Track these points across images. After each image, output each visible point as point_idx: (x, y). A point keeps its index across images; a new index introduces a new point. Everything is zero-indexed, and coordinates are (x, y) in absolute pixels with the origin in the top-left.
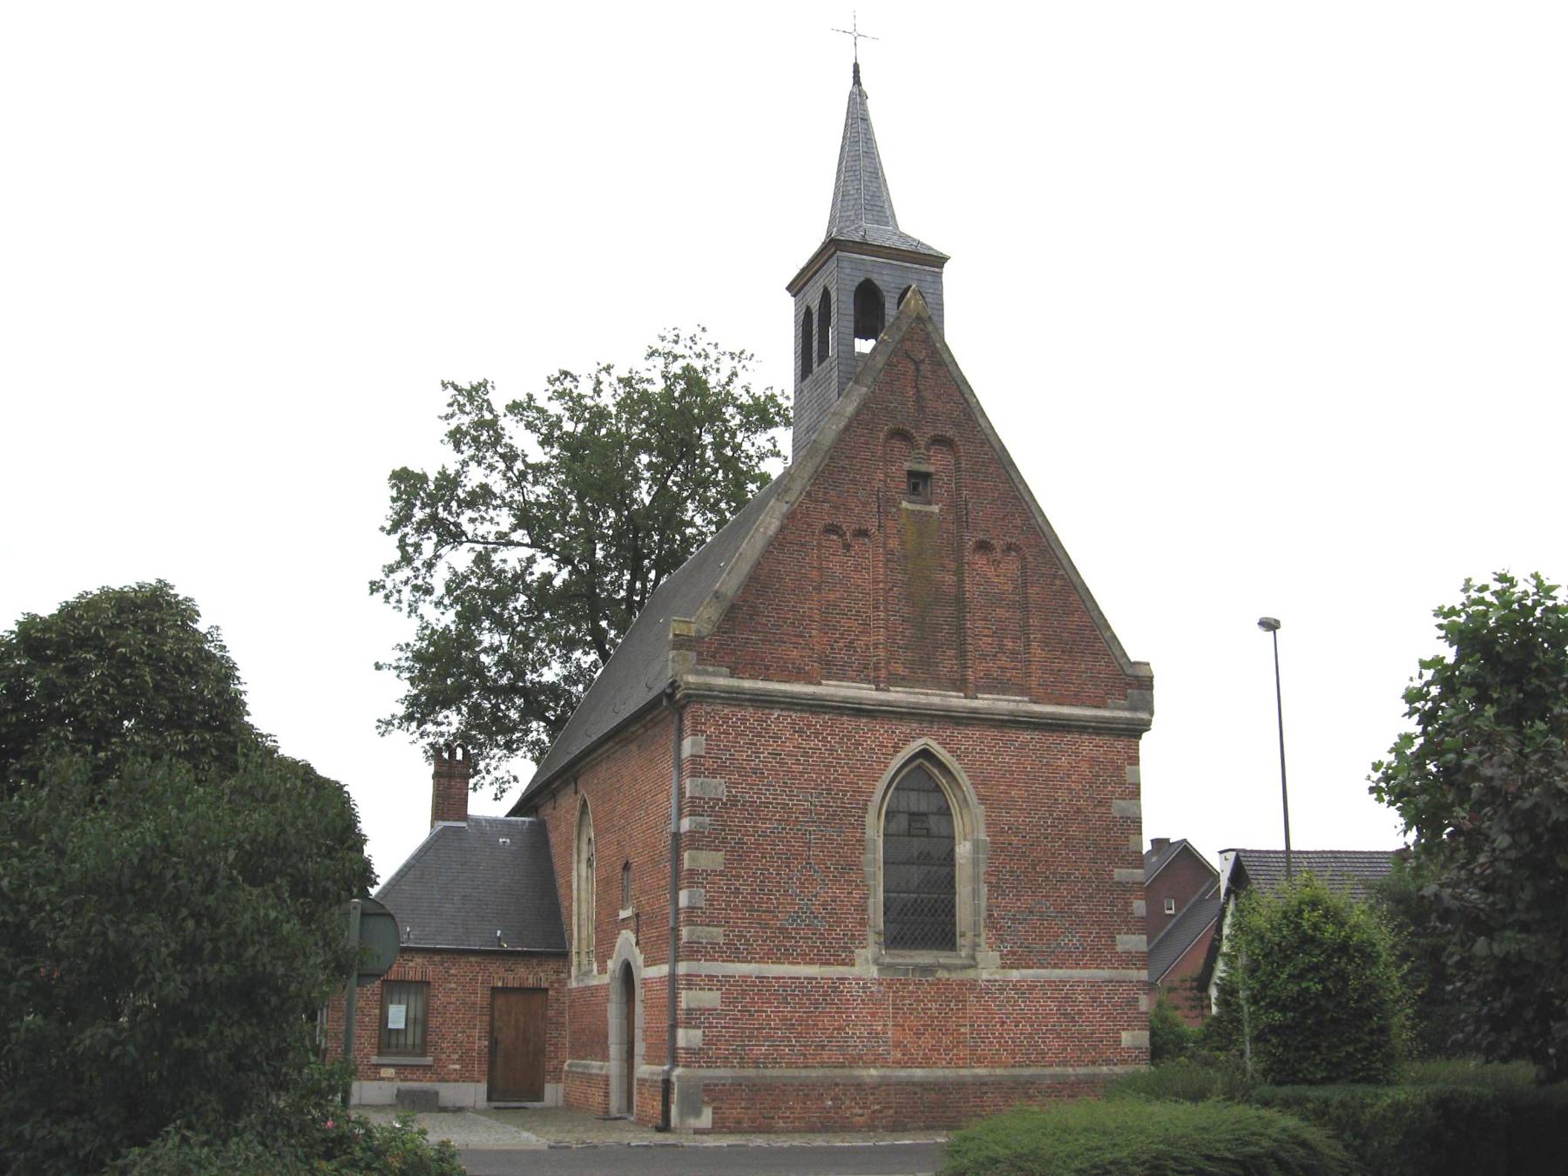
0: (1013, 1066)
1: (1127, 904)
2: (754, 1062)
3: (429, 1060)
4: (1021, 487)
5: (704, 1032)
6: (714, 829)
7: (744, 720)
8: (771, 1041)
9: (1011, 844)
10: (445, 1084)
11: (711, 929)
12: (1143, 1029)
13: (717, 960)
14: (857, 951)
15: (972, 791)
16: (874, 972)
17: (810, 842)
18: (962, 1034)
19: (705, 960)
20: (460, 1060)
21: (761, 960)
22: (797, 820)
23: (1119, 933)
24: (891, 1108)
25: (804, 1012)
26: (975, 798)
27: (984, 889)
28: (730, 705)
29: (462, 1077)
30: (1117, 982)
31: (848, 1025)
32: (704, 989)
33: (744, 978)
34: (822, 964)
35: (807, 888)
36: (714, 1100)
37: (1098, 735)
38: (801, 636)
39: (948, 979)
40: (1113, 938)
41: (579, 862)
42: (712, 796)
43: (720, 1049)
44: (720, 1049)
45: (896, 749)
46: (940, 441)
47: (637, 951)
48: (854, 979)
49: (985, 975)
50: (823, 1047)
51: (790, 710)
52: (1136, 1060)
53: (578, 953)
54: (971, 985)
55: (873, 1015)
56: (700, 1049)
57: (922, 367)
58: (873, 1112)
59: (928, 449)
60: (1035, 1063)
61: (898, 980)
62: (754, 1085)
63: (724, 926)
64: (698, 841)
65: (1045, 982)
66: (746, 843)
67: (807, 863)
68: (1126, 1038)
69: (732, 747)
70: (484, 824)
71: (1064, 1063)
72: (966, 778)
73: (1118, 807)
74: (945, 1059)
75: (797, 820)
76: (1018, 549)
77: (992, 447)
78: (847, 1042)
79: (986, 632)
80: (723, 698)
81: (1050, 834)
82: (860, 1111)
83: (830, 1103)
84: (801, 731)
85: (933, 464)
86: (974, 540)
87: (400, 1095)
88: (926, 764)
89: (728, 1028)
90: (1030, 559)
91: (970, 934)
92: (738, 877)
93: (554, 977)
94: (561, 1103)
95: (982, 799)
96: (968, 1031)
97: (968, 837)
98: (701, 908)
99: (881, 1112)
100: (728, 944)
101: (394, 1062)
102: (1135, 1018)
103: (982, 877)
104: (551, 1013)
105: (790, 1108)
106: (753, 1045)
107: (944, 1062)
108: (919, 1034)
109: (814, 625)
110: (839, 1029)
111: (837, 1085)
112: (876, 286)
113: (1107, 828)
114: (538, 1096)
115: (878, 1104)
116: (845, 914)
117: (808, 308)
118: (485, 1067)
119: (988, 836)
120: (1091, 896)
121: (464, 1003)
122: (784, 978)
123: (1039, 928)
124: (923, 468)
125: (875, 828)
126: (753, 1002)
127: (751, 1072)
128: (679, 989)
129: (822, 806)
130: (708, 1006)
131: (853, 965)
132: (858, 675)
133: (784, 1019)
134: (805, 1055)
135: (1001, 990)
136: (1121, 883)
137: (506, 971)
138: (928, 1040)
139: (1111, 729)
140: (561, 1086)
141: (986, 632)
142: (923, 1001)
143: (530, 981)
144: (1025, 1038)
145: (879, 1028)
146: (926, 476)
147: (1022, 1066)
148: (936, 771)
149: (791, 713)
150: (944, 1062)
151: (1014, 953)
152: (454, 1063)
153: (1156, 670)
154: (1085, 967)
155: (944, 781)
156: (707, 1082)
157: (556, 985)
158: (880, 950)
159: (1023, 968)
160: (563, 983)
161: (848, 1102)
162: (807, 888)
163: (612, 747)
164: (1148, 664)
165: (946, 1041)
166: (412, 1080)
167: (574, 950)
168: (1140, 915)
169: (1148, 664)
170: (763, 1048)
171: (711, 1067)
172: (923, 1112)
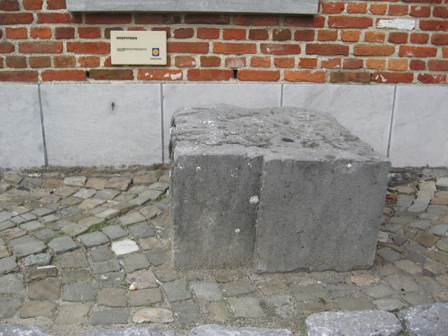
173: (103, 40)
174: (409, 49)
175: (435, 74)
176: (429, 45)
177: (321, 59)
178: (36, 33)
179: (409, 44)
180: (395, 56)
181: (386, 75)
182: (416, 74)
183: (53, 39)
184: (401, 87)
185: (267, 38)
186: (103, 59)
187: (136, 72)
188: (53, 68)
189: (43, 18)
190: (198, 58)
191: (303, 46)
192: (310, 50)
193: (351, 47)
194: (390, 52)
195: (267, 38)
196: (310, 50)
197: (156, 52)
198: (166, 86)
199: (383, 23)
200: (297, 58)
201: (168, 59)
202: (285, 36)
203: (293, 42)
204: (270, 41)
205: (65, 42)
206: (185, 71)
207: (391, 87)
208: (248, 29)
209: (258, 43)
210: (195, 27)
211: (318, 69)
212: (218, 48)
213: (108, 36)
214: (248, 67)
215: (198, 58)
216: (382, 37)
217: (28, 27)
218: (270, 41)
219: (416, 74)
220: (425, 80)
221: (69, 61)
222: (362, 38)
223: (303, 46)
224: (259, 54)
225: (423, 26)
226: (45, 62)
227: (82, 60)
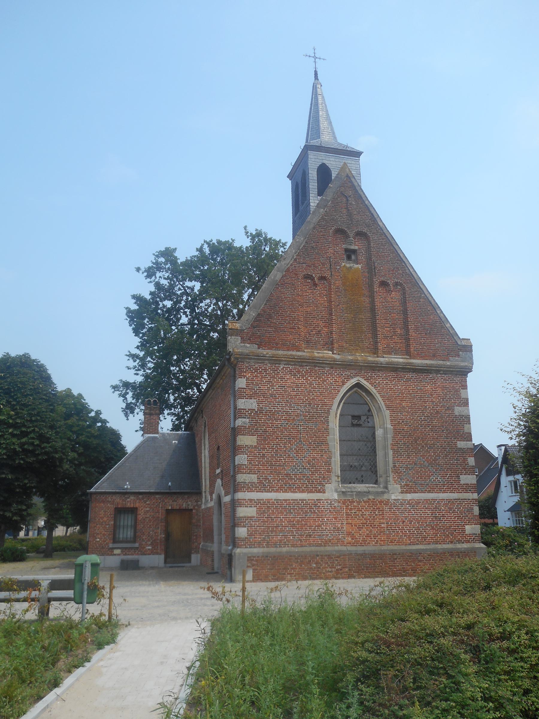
0: (410, 544)
1: (465, 460)
2: (274, 544)
3: (137, 545)
4: (401, 255)
5: (248, 529)
6: (251, 425)
7: (265, 370)
8: (283, 533)
9: (404, 430)
10: (144, 556)
11: (251, 475)
12: (476, 524)
13: (254, 491)
14: (326, 485)
15: (383, 403)
16: (336, 496)
17: (301, 431)
18: (382, 528)
19: (248, 492)
20: (152, 544)
21: (277, 491)
22: (294, 419)
23: (461, 474)
24: (346, 567)
25: (299, 518)
26: (384, 407)
27: (391, 453)
28: (258, 363)
29: (152, 552)
30: (461, 500)
31: (323, 524)
32: (247, 507)
33: (268, 500)
34: (308, 492)
35: (300, 453)
36: (253, 565)
37: (446, 374)
38: (294, 329)
39: (374, 499)
40: (458, 477)
41: (205, 449)
42: (250, 408)
43: (257, 538)
44: (257, 538)
45: (344, 383)
46: (360, 234)
47: (222, 489)
48: (325, 500)
49: (393, 497)
50: (310, 536)
51: (288, 364)
52: (474, 541)
53: (205, 492)
54: (386, 502)
55: (336, 518)
56: (246, 538)
57: (350, 199)
58: (337, 570)
59: (355, 238)
60: (421, 543)
61: (348, 500)
62: (275, 557)
63: (258, 474)
64: (243, 431)
65: (424, 500)
66: (268, 432)
67: (299, 441)
68: (469, 529)
69: (260, 383)
70: (166, 435)
71: (437, 543)
72: (379, 397)
73: (458, 410)
74: (374, 541)
75: (294, 419)
76: (401, 285)
77: (386, 236)
78: (322, 533)
79: (387, 325)
80: (254, 359)
81: (424, 424)
82: (330, 570)
83: (315, 565)
84: (295, 375)
85: (357, 245)
86: (379, 280)
87: (122, 562)
88: (359, 390)
89: (260, 526)
90: (407, 289)
91: (384, 476)
92: (264, 448)
93: (195, 504)
94: (199, 564)
95: (388, 407)
96: (385, 526)
97: (382, 427)
98: (246, 465)
99: (341, 570)
100: (260, 482)
101: (120, 546)
102: (472, 518)
103: (390, 447)
104: (194, 521)
105: (293, 569)
106: (274, 535)
107: (374, 543)
108: (360, 528)
109: (300, 323)
110: (319, 526)
111: (318, 556)
112: (328, 166)
113: (453, 421)
114: (190, 561)
115: (340, 565)
116: (320, 466)
117: (297, 183)
118: (163, 547)
119: (392, 426)
120: (446, 456)
121: (153, 517)
122: (289, 500)
123: (420, 472)
124: (353, 247)
125: (334, 423)
126: (273, 513)
127: (272, 550)
128: (235, 507)
129: (306, 412)
130: (250, 515)
131: (324, 493)
132: (323, 347)
133: (290, 521)
134: (301, 540)
135: (402, 504)
136: (461, 448)
137: (173, 501)
138: (365, 531)
139: (452, 371)
140: (199, 555)
141: (387, 325)
142: (361, 511)
143: (184, 506)
144: (415, 529)
145: (339, 525)
146: (354, 252)
147: (415, 545)
148: (364, 394)
149: (290, 366)
150: (374, 543)
151: (407, 485)
152: (149, 546)
153: (473, 342)
154: (444, 492)
155: (368, 399)
156: (249, 555)
157: (196, 507)
158: (339, 485)
159: (412, 493)
160: (200, 506)
161: (324, 565)
162: (300, 453)
163: (212, 392)
164: (469, 339)
165: (375, 531)
166: (129, 555)
167: (203, 490)
168: (472, 465)
169: (469, 339)
170: (279, 537)
171: (252, 547)
172: (363, 569)
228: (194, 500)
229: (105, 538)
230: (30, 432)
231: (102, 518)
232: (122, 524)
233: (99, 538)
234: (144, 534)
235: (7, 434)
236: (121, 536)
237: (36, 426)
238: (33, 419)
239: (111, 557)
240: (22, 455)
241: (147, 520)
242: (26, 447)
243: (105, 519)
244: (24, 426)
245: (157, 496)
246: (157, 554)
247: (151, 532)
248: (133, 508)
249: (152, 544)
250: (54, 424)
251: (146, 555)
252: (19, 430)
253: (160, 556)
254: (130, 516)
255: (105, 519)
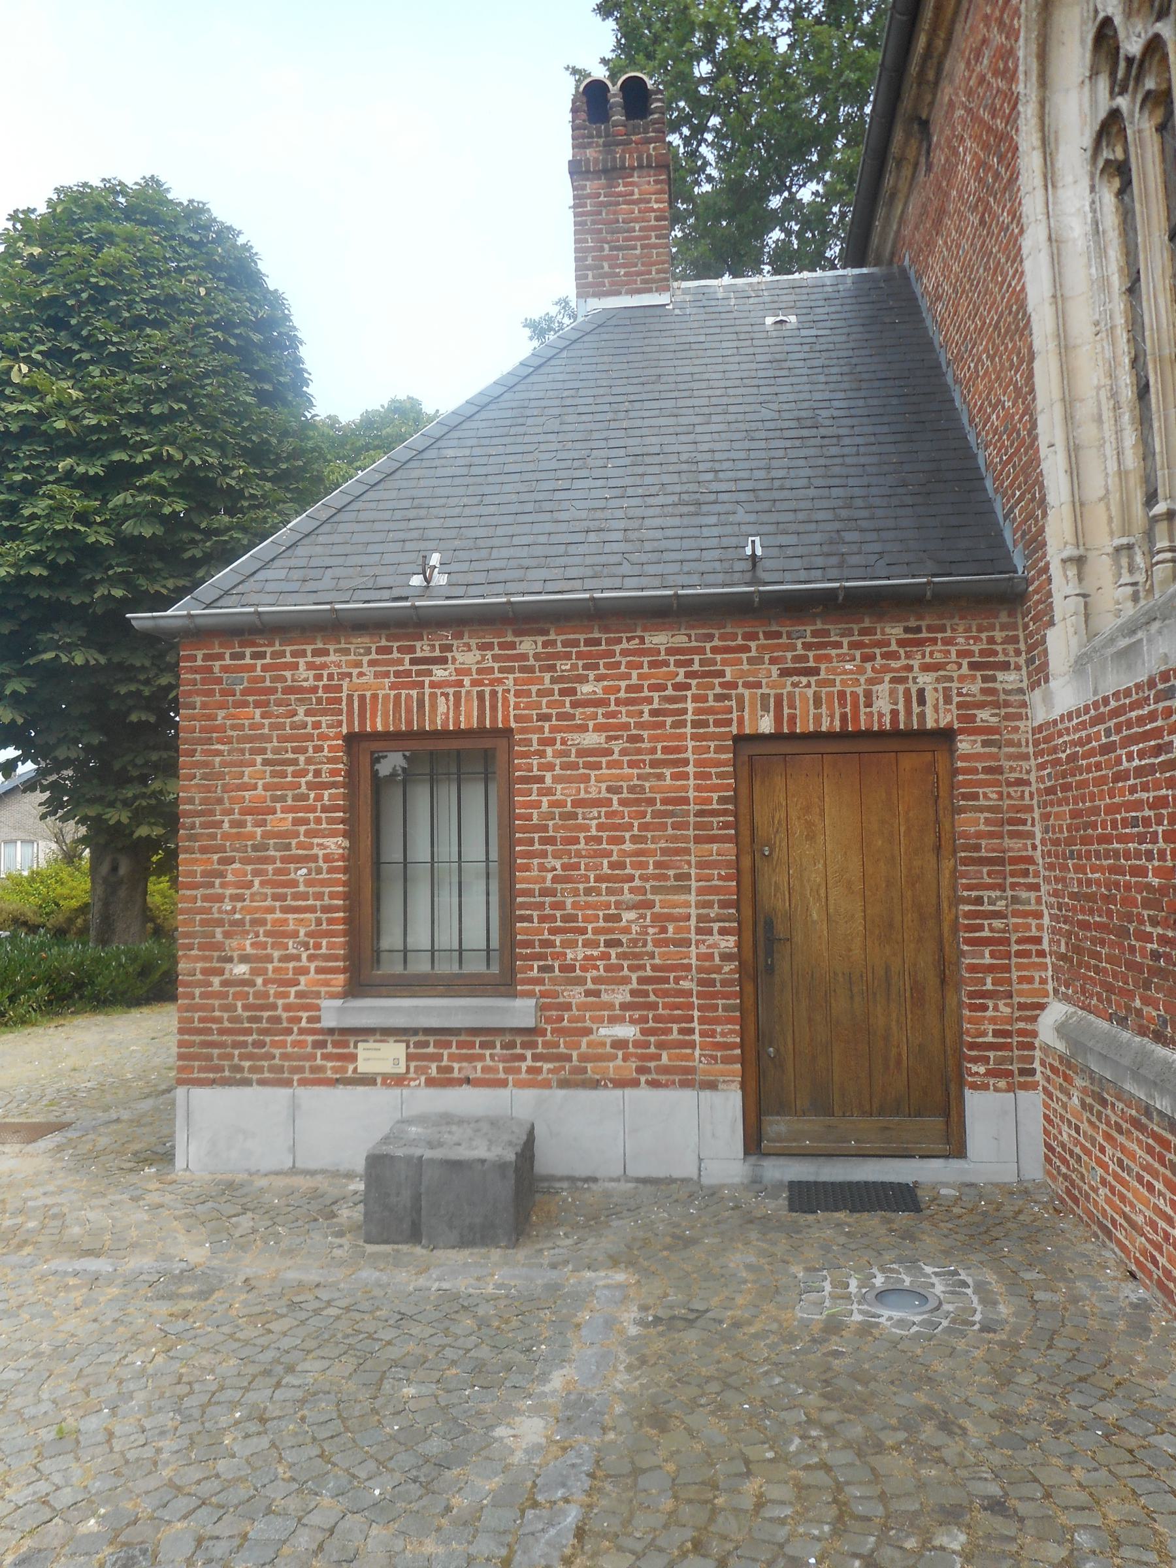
20: (637, 1006)
41: (1050, 179)
53: (1079, 561)
104: (971, 823)
118: (728, 1033)
137: (785, 673)
140: (1032, 1102)
143: (882, 705)
157: (984, 716)
173: (351, 1050)
174: (632, 1055)
175: (663, 1078)
176: (652, 1050)
177: (547, 1066)
178: (295, 1044)
179: (631, 1050)
180: (619, 1062)
181: (611, 1080)
182: (643, 1079)
183: (309, 1049)
184: (629, 1092)
185: (494, 1047)
186: (351, 1067)
187: (379, 1080)
188: (307, 1075)
189: (302, 1031)
190: (434, 1066)
191: (529, 1054)
192: (535, 1058)
193: (575, 1054)
194: (614, 1057)
195: (494, 1047)
196: (535, 1058)
197: (396, 1061)
198: (406, 1092)
199: (602, 1031)
200: (524, 1066)
201: (408, 1068)
202: (511, 1045)
203: (519, 1051)
204: (498, 1050)
205: (319, 1053)
206: (423, 1079)
207: (618, 1093)
208: (478, 1040)
209: (488, 1052)
210: (431, 1039)
211: (544, 1075)
212: (452, 1057)
213: (356, 1047)
214: (479, 1074)
215: (434, 1066)
216: (603, 1044)
217: (289, 1039)
218: (498, 1050)
219: (643, 1079)
220: (654, 1084)
221: (321, 1069)
222: (584, 1045)
223: (529, 1054)
224: (489, 1062)
225: (644, 1032)
226: (300, 1070)
227: (332, 1068)
228: (961, 654)
229: (285, 959)
230: (146, 468)
231: (260, 812)
232: (421, 851)
233: (244, 959)
234: (571, 927)
235: (51, 478)
236: (420, 938)
237: (170, 440)
238: (156, 410)
239: (341, 1093)
240: (118, 565)
241: (592, 819)
242: (128, 527)
243: (281, 820)
244: (122, 443)
245: (659, 639)
246: (685, 1084)
247: (628, 916)
248: (481, 732)
249: (637, 1006)
250: (266, 442)
251: (595, 1084)
252: (99, 463)
253: (706, 1095)
254: (474, 795)
255: (281, 820)
